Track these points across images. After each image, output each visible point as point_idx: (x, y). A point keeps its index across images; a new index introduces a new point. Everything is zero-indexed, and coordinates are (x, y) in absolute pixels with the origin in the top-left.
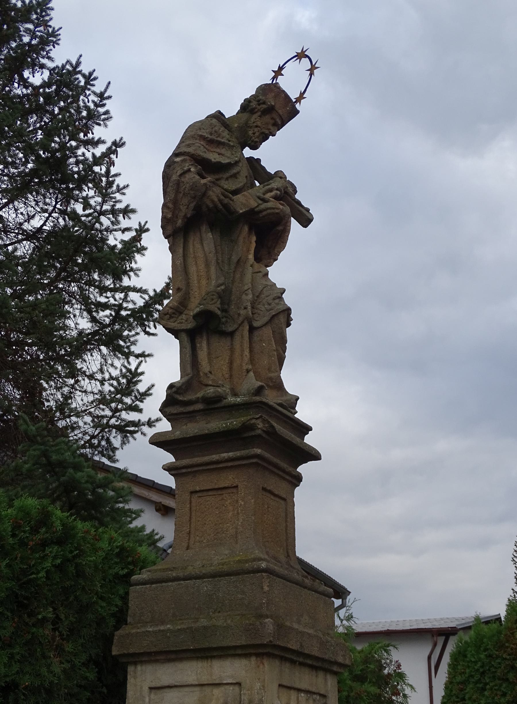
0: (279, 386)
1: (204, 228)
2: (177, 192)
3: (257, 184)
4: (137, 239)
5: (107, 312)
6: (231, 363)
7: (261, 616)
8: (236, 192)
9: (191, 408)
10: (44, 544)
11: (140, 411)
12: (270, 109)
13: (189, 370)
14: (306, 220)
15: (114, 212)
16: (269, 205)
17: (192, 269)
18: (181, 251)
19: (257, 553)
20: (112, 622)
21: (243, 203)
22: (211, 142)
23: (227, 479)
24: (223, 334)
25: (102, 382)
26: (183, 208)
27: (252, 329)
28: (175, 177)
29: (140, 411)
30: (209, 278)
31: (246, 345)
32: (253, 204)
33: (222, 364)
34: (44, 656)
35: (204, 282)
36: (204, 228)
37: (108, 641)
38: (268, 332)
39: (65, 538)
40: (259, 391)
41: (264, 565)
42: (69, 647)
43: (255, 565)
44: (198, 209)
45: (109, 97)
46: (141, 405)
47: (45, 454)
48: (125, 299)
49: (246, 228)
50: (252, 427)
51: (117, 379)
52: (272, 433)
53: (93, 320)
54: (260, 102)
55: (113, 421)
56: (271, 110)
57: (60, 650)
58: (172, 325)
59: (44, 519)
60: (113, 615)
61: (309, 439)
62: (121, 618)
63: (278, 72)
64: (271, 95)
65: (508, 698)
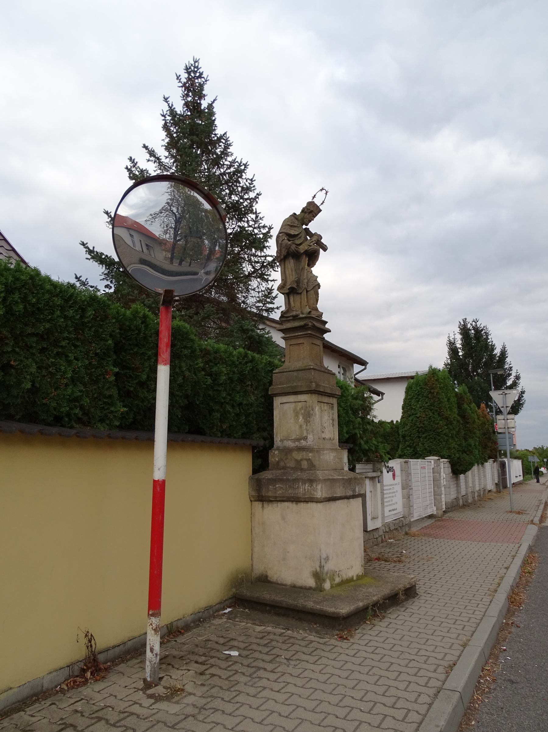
0: (317, 309)
1: (290, 258)
2: (281, 247)
3: (309, 238)
4: (269, 232)
5: (259, 264)
6: (301, 302)
7: (312, 382)
8: (301, 244)
9: (289, 319)
10: (246, 363)
11: (274, 303)
12: (311, 211)
13: (287, 306)
14: (325, 249)
15: (259, 227)
16: (312, 247)
17: (287, 272)
18: (283, 267)
19: (310, 363)
20: (268, 384)
21: (302, 249)
22: (292, 226)
23: (301, 341)
24: (298, 294)
25: (259, 292)
26: (283, 252)
27: (307, 291)
28: (280, 242)
29: (274, 303)
30: (292, 275)
31: (305, 297)
32: (306, 248)
33: (298, 304)
34: (249, 395)
35: (291, 277)
36: (290, 258)
37: (267, 390)
38: (312, 292)
39: (253, 360)
40: (310, 312)
41: (312, 367)
42: (256, 392)
43: (309, 367)
44: (288, 253)
45: (255, 180)
46: (274, 301)
47: (241, 327)
48: (265, 259)
49: (304, 256)
50: (308, 325)
51: (264, 291)
52: (314, 326)
53: (253, 267)
54: (308, 209)
55: (264, 308)
56: (311, 212)
57: (253, 393)
58: (281, 291)
59: (246, 355)
60: (268, 382)
61: (327, 326)
62: (271, 383)
63: (314, 197)
64: (312, 206)
65: (428, 404)
